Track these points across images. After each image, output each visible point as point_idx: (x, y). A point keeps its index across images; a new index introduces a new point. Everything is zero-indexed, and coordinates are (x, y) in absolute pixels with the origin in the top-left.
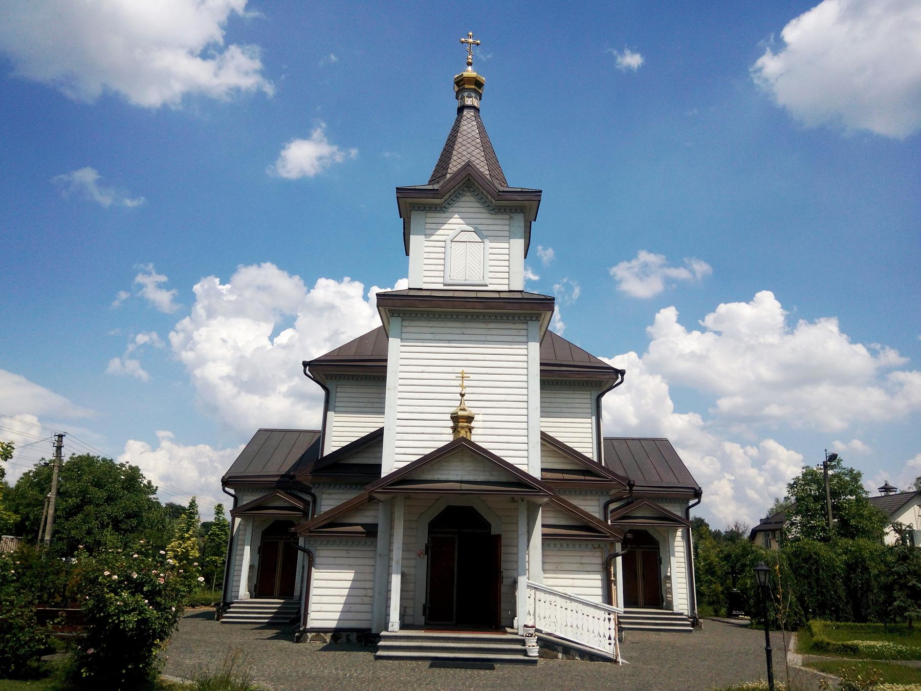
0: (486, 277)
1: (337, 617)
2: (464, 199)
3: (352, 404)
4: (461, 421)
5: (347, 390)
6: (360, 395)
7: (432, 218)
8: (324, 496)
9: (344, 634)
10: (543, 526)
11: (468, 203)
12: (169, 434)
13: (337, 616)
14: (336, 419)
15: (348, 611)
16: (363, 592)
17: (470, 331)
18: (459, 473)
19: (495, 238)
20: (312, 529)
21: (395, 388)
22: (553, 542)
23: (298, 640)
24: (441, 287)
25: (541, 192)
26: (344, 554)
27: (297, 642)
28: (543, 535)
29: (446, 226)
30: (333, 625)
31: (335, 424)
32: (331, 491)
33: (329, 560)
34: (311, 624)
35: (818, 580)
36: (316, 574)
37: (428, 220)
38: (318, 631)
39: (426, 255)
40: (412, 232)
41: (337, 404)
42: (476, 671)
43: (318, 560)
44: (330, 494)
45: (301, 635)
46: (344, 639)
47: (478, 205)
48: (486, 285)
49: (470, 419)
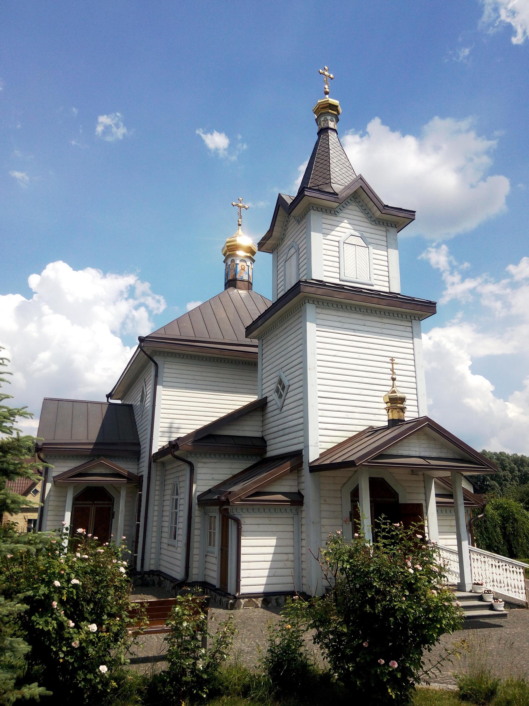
0: (372, 279)
1: (264, 582)
2: (350, 207)
3: (178, 380)
4: (396, 402)
5: (174, 367)
6: (185, 372)
7: (328, 219)
8: (200, 465)
9: (274, 598)
10: (437, 495)
11: (353, 211)
12: (470, 402)
13: (264, 581)
14: (164, 393)
15: (274, 576)
16: (285, 557)
17: (368, 323)
18: (417, 449)
19: (377, 246)
20: (243, 498)
21: (314, 368)
22: (448, 509)
23: (233, 607)
24: (337, 281)
25: (414, 212)
26: (267, 521)
27: (231, 609)
28: (437, 503)
29: (338, 229)
30: (260, 589)
31: (164, 397)
32: (204, 460)
33: (255, 528)
34: (244, 590)
35: (486, 528)
36: (244, 542)
37: (324, 221)
38: (251, 596)
39: (324, 252)
40: (312, 229)
41: (164, 379)
42: (475, 630)
43: (244, 528)
44: (204, 463)
45: (235, 602)
46: (274, 602)
47: (361, 214)
48: (372, 285)
49: (403, 400)
